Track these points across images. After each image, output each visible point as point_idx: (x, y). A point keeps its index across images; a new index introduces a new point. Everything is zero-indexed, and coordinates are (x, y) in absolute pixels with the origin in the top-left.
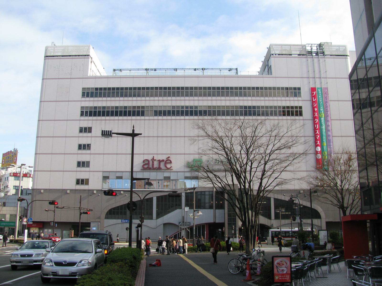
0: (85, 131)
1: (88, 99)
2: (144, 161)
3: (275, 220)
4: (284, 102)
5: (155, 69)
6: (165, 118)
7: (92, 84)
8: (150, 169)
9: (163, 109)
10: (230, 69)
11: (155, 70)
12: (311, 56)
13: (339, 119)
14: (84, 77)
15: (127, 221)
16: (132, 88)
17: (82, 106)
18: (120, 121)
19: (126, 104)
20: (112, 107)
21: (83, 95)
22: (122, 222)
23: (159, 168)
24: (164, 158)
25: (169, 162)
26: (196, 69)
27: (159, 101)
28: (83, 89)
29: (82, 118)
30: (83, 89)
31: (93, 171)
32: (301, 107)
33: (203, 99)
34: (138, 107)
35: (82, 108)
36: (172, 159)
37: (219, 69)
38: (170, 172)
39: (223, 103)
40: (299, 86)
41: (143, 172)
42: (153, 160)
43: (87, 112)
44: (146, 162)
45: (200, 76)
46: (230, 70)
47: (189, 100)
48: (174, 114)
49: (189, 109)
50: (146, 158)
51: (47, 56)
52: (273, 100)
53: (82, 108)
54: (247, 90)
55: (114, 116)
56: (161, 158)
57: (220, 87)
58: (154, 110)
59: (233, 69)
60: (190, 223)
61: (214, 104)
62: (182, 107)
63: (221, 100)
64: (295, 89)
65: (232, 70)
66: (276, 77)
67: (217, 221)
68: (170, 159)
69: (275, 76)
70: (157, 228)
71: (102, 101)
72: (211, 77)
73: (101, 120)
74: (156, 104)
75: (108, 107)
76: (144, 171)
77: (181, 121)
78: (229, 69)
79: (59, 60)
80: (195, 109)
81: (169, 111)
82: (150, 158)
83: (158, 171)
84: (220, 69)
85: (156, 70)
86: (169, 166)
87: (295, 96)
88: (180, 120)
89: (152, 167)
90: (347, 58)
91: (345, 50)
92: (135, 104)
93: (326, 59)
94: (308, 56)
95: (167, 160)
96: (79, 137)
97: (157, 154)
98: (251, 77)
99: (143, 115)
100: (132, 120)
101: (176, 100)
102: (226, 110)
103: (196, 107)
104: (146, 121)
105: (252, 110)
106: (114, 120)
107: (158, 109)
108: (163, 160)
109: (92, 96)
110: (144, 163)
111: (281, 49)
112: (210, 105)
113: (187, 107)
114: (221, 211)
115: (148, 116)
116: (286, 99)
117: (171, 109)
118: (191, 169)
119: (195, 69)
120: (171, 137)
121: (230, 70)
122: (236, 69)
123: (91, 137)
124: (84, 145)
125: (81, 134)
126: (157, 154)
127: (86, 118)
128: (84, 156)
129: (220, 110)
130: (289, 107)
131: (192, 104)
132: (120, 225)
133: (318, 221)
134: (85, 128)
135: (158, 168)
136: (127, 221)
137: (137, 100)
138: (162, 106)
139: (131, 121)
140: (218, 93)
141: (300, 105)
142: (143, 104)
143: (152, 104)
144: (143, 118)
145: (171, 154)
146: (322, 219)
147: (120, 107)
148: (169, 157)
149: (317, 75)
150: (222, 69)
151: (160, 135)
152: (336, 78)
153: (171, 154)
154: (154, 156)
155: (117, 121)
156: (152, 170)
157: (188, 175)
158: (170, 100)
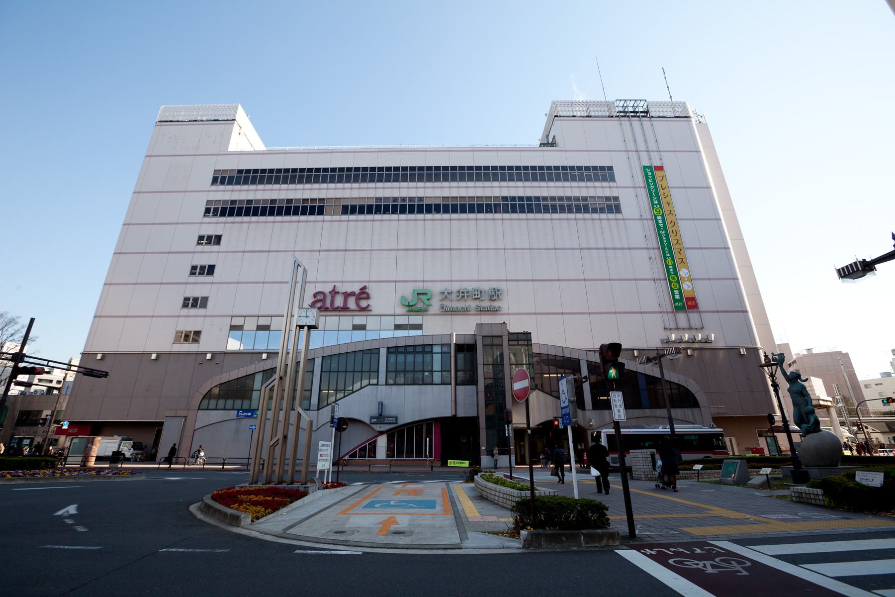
1: (222, 187)
2: (315, 295)
3: (593, 411)
8: (327, 309)
9: (357, 203)
14: (220, 153)
15: (249, 414)
16: (376, 167)
17: (208, 199)
19: (291, 195)
20: (265, 201)
22: (237, 416)
23: (345, 309)
24: (356, 289)
31: (213, 316)
32: (616, 199)
34: (313, 200)
36: (372, 290)
38: (367, 316)
39: (471, 193)
42: (334, 293)
43: (216, 210)
45: (358, 150)
47: (408, 188)
48: (446, 211)
50: (320, 288)
55: (373, 214)
56: (349, 288)
57: (456, 167)
58: (342, 204)
60: (396, 418)
61: (455, 193)
62: (395, 199)
63: (467, 187)
64: (602, 168)
67: (461, 414)
68: (367, 291)
69: (564, 149)
70: (317, 430)
72: (449, 151)
73: (365, 221)
75: (258, 201)
82: (327, 289)
83: (342, 313)
86: (364, 304)
88: (442, 220)
89: (329, 307)
90: (691, 121)
91: (685, 108)
92: (308, 195)
93: (653, 122)
97: (342, 282)
98: (520, 151)
100: (373, 221)
101: (384, 188)
102: (451, 204)
103: (421, 199)
107: (350, 203)
108: (353, 294)
110: (315, 299)
114: (471, 388)
115: (330, 214)
117: (374, 203)
118: (407, 309)
126: (342, 282)
127: (215, 219)
128: (199, 287)
129: (483, 204)
131: (413, 193)
132: (233, 423)
133: (692, 412)
134: (209, 238)
136: (249, 414)
140: (542, 175)
141: (615, 195)
143: (339, 194)
144: (320, 218)
145: (369, 282)
146: (702, 408)
147: (279, 200)
148: (365, 288)
149: (642, 146)
151: (350, 247)
153: (369, 282)
154: (335, 286)
155: (271, 224)
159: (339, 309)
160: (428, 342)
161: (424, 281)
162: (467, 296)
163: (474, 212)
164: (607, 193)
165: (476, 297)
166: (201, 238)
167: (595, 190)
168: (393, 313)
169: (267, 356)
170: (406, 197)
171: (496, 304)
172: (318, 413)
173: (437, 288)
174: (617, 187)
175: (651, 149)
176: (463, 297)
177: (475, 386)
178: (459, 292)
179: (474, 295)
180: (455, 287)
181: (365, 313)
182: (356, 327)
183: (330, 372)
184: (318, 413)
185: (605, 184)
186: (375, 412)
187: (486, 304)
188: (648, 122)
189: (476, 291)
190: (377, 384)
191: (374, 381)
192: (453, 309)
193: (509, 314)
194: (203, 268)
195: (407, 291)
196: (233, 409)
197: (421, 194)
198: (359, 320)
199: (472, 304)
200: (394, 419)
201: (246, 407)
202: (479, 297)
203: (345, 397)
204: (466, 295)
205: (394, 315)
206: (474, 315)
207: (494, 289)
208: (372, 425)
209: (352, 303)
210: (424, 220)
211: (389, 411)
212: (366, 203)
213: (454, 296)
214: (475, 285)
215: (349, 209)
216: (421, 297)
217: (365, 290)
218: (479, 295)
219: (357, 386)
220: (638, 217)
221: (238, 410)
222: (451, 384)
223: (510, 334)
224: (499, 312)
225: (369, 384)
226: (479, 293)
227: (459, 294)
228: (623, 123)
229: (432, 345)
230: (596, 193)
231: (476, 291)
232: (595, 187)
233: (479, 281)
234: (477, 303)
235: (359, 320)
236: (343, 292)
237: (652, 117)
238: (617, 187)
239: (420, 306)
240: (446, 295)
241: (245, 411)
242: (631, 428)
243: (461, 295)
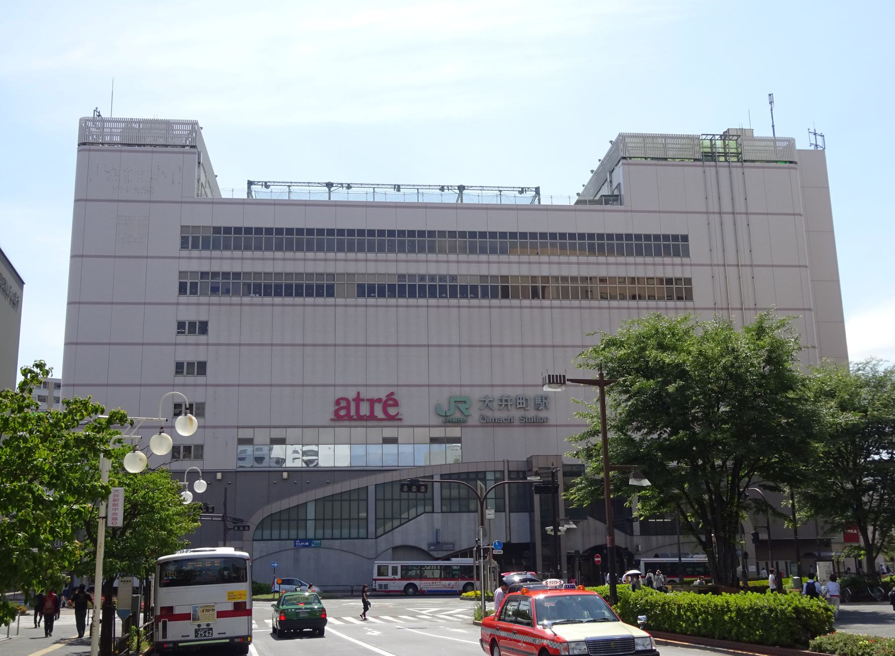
0: (192, 329)
4: (613, 268)
5: (348, 184)
6: (382, 301)
7: (204, 218)
8: (350, 418)
9: (376, 282)
10: (522, 188)
11: (349, 187)
12: (713, 163)
13: (802, 307)
15: (307, 544)
18: (245, 308)
21: (182, 243)
22: (295, 546)
23: (372, 417)
24: (382, 394)
25: (390, 402)
26: (445, 188)
27: (429, 264)
28: (184, 228)
29: (183, 299)
30: (184, 228)
31: (214, 427)
32: (688, 281)
33: (501, 260)
35: (182, 274)
36: (401, 395)
37: (497, 189)
38: (398, 427)
40: (685, 233)
41: (334, 427)
42: (358, 400)
44: (343, 404)
46: (522, 191)
49: (580, 285)
50: (340, 393)
51: (84, 144)
52: (417, 261)
53: (182, 274)
54: (356, 238)
56: (373, 394)
58: (356, 282)
59: (528, 188)
60: (453, 544)
62: (422, 278)
63: (509, 263)
64: (675, 238)
65: (526, 191)
66: (632, 211)
67: (513, 541)
71: (232, 259)
74: (361, 268)
76: (337, 423)
77: (359, 308)
78: (520, 189)
79: (181, 156)
80: (452, 282)
81: (392, 287)
82: (351, 394)
84: (500, 189)
85: (351, 187)
86: (392, 411)
87: (677, 254)
93: (745, 169)
94: (707, 163)
95: (386, 401)
96: (176, 344)
97: (366, 386)
99: (331, 294)
101: (253, 259)
103: (453, 278)
104: (554, 310)
105: (551, 285)
106: (262, 305)
107: (366, 281)
108: (379, 400)
109: (206, 247)
111: (643, 145)
112: (484, 272)
113: (432, 278)
116: (561, 261)
117: (395, 281)
119: (443, 187)
120: (397, 346)
121: (521, 192)
122: (536, 188)
123: (208, 344)
124: (188, 364)
125: (182, 339)
126: (366, 386)
130: (672, 279)
134: (192, 324)
135: (367, 417)
136: (307, 544)
137: (315, 260)
138: (344, 274)
139: (302, 308)
141: (687, 275)
142: (330, 268)
143: (351, 268)
144: (330, 300)
148: (392, 394)
149: (727, 207)
150: (504, 189)
152: (659, 212)
153: (398, 386)
156: (355, 420)
157: (438, 433)
158: (423, 261)
159: (365, 418)
160: (481, 468)
161: (461, 386)
162: (511, 405)
163: (384, 296)
164: (677, 273)
165: (521, 406)
166: (181, 325)
167: (664, 269)
168: (427, 424)
169: (288, 475)
170: (436, 276)
171: (542, 414)
172: (376, 542)
173: (476, 394)
174: (691, 265)
175: (737, 210)
176: (507, 405)
177: (527, 514)
178: (501, 400)
179: (518, 404)
180: (497, 393)
181: (395, 423)
182: (387, 441)
183: (384, 500)
184: (376, 542)
185: (677, 260)
186: (432, 540)
187: (531, 413)
188: (740, 170)
189: (521, 399)
190: (433, 512)
191: (428, 509)
192: (495, 420)
193: (556, 426)
194: (191, 365)
195: (443, 396)
196: (289, 539)
197: (453, 271)
198: (389, 433)
199: (516, 414)
200: (451, 546)
201: (302, 535)
202: (524, 406)
203: (401, 525)
204: (509, 403)
205: (429, 426)
206: (518, 426)
207: (542, 397)
208: (430, 552)
209: (379, 411)
210: (273, 305)
211: (444, 538)
212: (387, 281)
213: (495, 405)
214: (519, 391)
215: (367, 290)
216: (460, 405)
217: (393, 397)
218: (524, 403)
219: (413, 512)
220: (712, 306)
221: (295, 540)
222: (504, 511)
223: (564, 465)
224: (545, 424)
225: (425, 513)
226: (524, 401)
227: (502, 402)
228: (708, 169)
229: (485, 472)
230: (664, 273)
231: (521, 399)
232: (664, 265)
233: (524, 386)
234: (521, 413)
235: (389, 433)
236: (368, 398)
237: (745, 161)
238: (691, 265)
239: (458, 415)
240: (486, 403)
241: (302, 540)
242: (669, 557)
243: (504, 403)
